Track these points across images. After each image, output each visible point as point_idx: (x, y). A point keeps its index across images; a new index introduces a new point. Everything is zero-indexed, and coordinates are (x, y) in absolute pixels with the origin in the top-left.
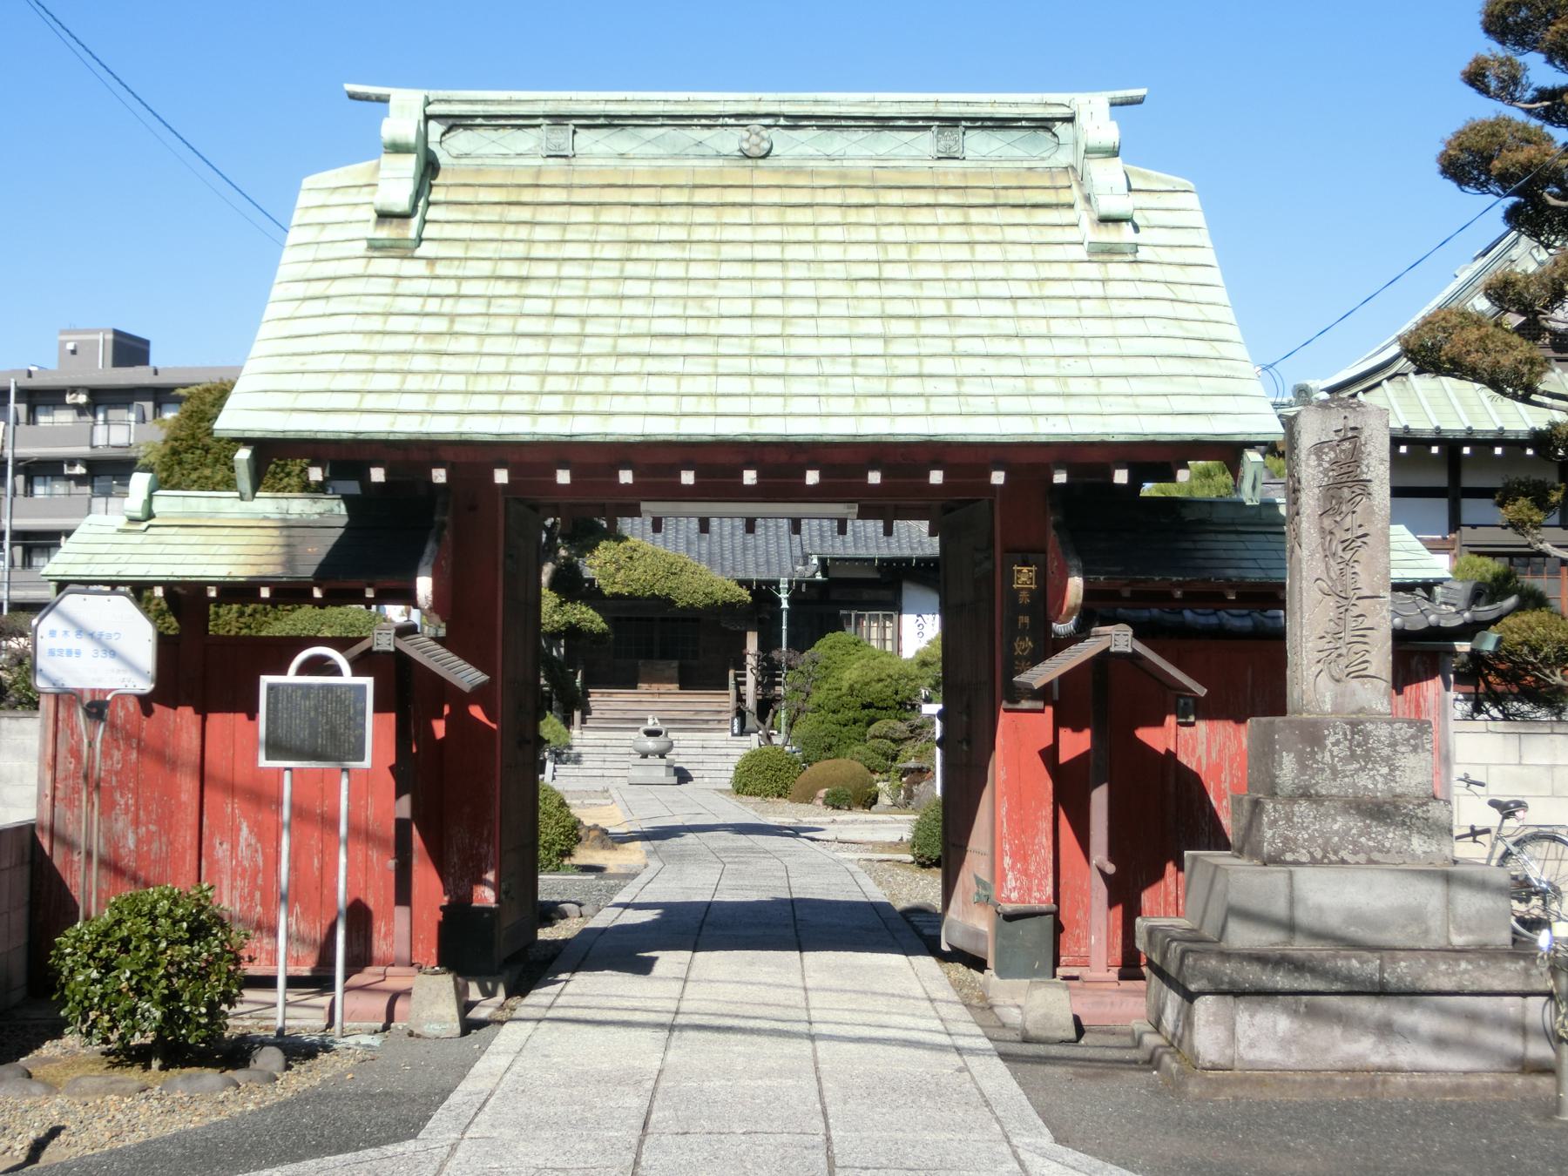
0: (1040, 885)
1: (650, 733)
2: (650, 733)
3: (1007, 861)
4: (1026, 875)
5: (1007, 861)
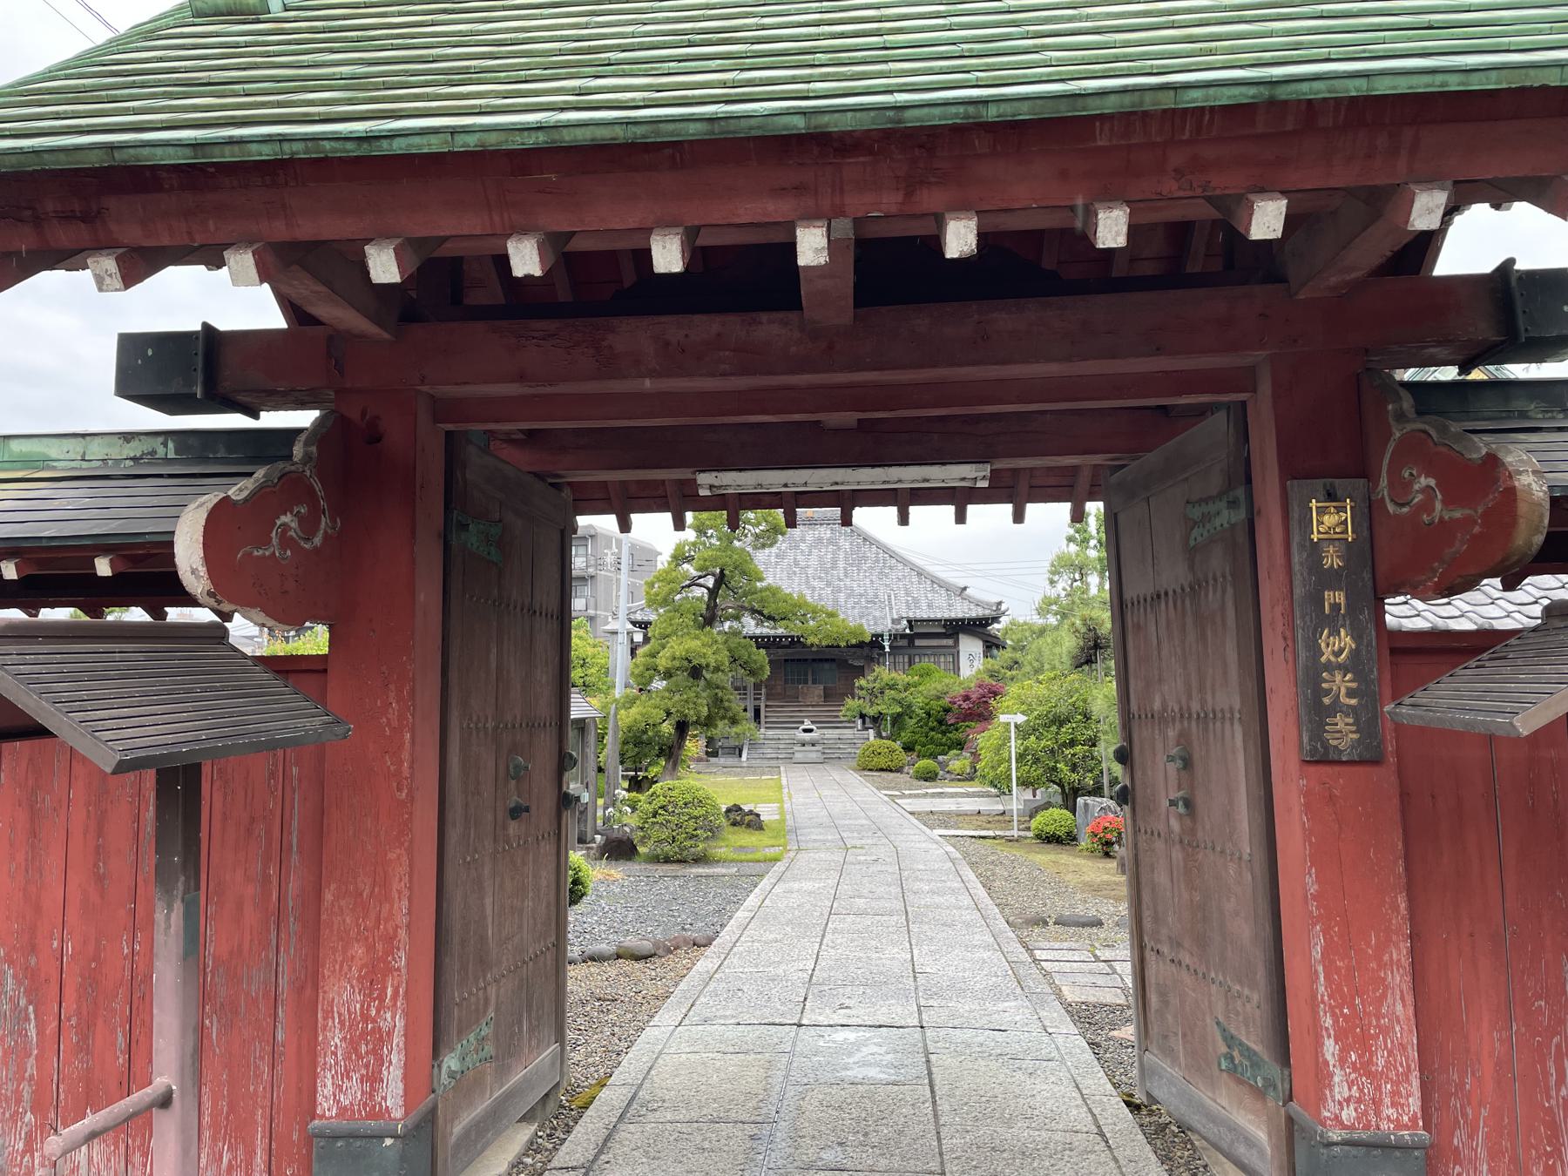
0: (1395, 1093)
1: (805, 731)
2: (805, 731)
3: (1330, 1048)
4: (1369, 1074)
5: (1330, 1048)
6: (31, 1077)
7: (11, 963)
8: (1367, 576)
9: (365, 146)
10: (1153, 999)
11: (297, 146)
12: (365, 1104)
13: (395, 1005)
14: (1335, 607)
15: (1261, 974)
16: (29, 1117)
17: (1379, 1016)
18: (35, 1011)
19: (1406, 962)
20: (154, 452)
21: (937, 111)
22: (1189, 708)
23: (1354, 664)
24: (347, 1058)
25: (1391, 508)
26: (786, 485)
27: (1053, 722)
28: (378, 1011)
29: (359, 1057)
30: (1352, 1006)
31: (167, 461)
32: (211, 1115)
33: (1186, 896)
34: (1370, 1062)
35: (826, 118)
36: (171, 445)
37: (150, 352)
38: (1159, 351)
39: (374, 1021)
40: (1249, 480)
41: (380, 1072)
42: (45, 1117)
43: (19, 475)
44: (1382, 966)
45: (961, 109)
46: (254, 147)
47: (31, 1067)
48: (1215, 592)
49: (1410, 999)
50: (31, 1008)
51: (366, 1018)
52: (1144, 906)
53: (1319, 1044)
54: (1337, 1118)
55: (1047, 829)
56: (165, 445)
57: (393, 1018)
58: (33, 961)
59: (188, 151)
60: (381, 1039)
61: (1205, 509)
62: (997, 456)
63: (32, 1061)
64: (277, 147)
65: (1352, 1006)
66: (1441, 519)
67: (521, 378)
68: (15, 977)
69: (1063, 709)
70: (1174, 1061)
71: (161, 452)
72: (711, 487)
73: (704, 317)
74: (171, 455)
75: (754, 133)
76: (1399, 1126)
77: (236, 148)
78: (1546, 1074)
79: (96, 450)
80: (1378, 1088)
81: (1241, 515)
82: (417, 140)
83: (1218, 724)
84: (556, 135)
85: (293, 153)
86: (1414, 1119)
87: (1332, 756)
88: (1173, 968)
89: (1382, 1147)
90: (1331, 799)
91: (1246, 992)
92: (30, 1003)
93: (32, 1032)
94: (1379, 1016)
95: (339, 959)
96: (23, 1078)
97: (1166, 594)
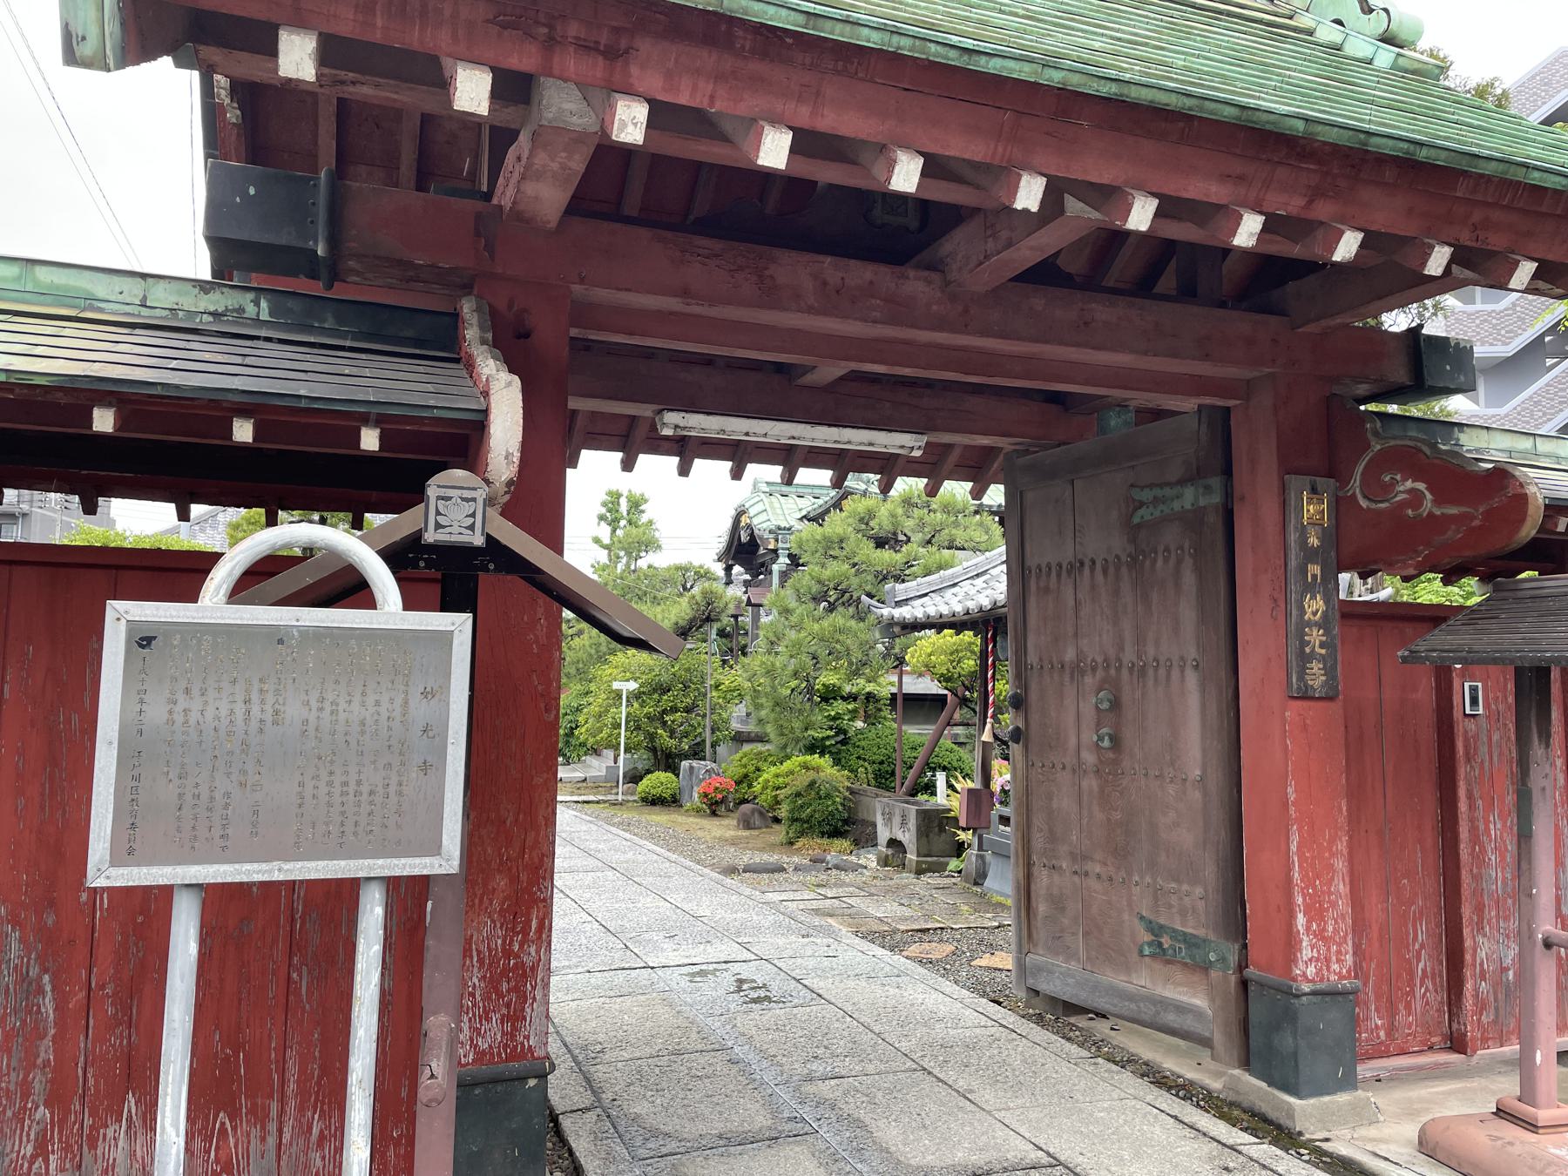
0: (1339, 952)
4: (1324, 939)
5: (1301, 920)
6: (46, 1063)
7: (16, 922)
8: (1333, 554)
9: (966, 57)
10: (1042, 908)
11: (905, 42)
12: (506, 1046)
13: (540, 937)
14: (1314, 577)
15: (1210, 871)
16: (43, 1113)
17: (1330, 893)
18: (51, 981)
19: (1345, 852)
20: (241, 310)
21: (1391, 142)
22: (1119, 660)
23: (1324, 624)
24: (486, 997)
25: (1364, 503)
26: (747, 434)
27: (655, 690)
28: (521, 946)
29: (500, 995)
30: (1314, 888)
31: (257, 321)
32: (298, 1082)
33: (1099, 816)
34: (1324, 930)
35: (1320, 128)
36: (264, 304)
37: (252, 191)
38: (1206, 357)
39: (517, 956)
40: (1228, 471)
41: (523, 1010)
42: (66, 1112)
43: (72, 313)
44: (1333, 855)
45: (1405, 146)
46: (866, 31)
47: (46, 1050)
48: (1166, 560)
49: (1347, 880)
50: (46, 978)
51: (508, 953)
52: (1034, 829)
53: (1292, 916)
54: (1304, 974)
55: (653, 792)
56: (257, 303)
57: (538, 952)
58: (50, 920)
59: (801, 19)
60: (524, 975)
61: (1158, 492)
62: (935, 429)
63: (47, 1042)
64: (886, 36)
65: (1314, 888)
66: (1431, 515)
67: (685, 293)
68: (22, 940)
69: (665, 678)
70: (1070, 955)
71: (251, 310)
72: (676, 427)
73: (858, 263)
74: (265, 316)
75: (1268, 127)
76: (1341, 977)
77: (848, 28)
78: (1408, 934)
79: (162, 297)
80: (1329, 949)
81: (1216, 498)
82: (1011, 64)
83: (1056, 676)
84: (1125, 90)
85: (899, 48)
86: (1349, 972)
87: (1310, 693)
88: (1076, 879)
89: (1333, 994)
90: (1305, 727)
91: (1185, 887)
92: (46, 971)
93: (48, 1006)
94: (1330, 893)
95: (479, 893)
96: (34, 1065)
97: (1093, 562)
